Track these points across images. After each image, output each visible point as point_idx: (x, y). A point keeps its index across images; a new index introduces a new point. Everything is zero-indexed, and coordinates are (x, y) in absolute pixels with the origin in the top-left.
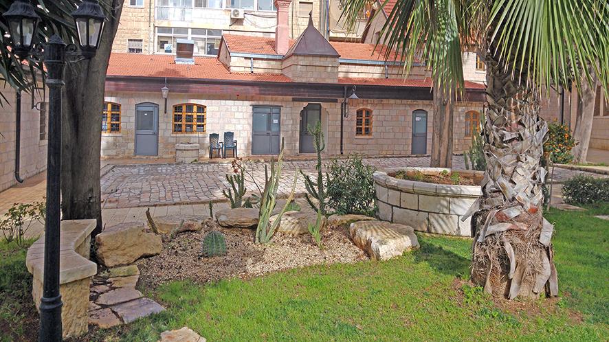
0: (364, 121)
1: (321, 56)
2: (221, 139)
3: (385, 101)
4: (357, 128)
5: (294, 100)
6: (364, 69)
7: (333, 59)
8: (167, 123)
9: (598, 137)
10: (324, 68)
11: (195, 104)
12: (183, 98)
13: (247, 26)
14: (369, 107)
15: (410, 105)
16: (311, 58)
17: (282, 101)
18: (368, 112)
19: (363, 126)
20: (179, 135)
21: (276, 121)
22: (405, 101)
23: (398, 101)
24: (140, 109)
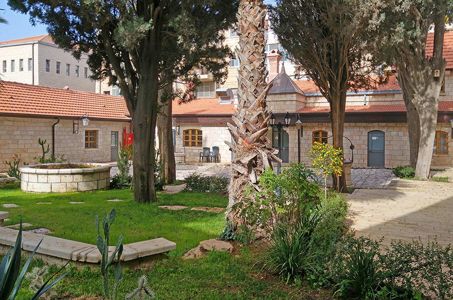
1: (280, 94)
7: (291, 95)
12: (195, 125)
15: (364, 127)
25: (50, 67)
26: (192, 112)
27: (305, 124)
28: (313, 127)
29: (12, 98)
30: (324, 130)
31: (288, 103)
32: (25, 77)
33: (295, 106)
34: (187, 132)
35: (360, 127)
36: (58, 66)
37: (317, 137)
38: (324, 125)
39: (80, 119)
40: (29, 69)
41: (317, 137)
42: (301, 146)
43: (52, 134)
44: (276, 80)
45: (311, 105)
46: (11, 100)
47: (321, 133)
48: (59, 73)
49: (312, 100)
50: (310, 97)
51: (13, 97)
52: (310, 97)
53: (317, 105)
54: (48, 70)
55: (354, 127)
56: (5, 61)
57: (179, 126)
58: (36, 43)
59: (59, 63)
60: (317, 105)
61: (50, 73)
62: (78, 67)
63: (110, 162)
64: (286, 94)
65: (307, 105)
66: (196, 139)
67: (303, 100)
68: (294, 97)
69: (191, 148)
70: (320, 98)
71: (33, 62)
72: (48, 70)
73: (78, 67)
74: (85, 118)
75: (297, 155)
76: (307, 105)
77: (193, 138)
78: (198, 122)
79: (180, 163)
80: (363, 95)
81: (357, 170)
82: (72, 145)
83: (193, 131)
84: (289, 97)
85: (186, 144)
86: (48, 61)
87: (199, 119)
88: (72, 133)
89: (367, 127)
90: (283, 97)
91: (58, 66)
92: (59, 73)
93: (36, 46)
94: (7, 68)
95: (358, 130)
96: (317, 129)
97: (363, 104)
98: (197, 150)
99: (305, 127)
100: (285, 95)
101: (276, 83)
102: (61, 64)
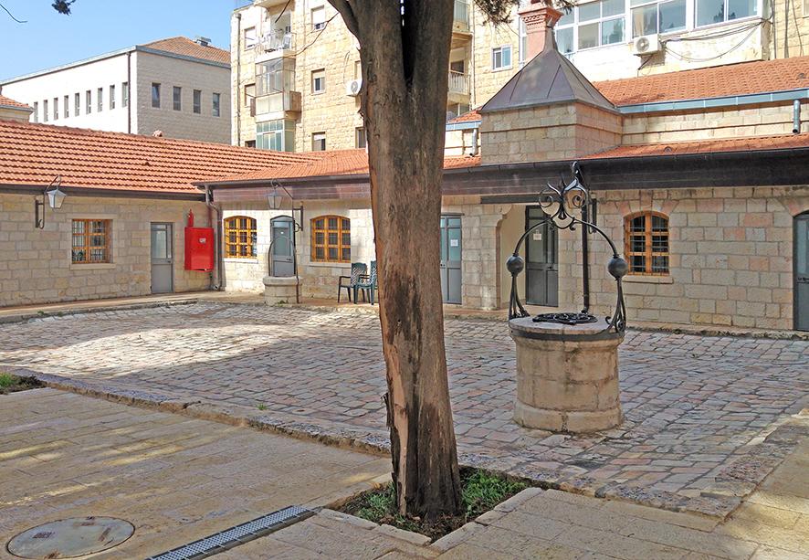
0: (648, 241)
1: (534, 108)
2: (517, 267)
3: (702, 192)
4: (666, 250)
5: (484, 201)
6: (729, 117)
7: (563, 109)
8: (304, 245)
9: (704, 533)
10: (541, 132)
11: (324, 217)
12: (330, 206)
13: (672, 64)
14: (656, 209)
15: (780, 199)
16: (515, 115)
17: (463, 205)
18: (661, 222)
19: (647, 254)
20: (320, 264)
21: (454, 243)
22: (765, 190)
23: (744, 191)
24: (277, 225)
25: (161, 97)
26: (323, 173)
27: (598, 194)
28: (626, 202)
29: (147, 164)
30: (638, 210)
31: (554, 133)
32: (114, 120)
33: (573, 143)
34: (317, 222)
35: (766, 200)
36: (177, 96)
37: (639, 234)
38: (656, 195)
39: (43, 190)
40: (124, 105)
41: (639, 234)
42: (591, 261)
43: (589, 242)
44: (528, 71)
45: (637, 140)
46: (147, 167)
47: (648, 222)
48: (179, 110)
49: (639, 125)
50: (632, 116)
51: (150, 163)
52: (632, 116)
53: (653, 139)
54: (156, 104)
55: (746, 199)
56: (89, 92)
57: (302, 209)
58: (133, 51)
59: (180, 88)
60: (653, 139)
61: (161, 109)
62: (219, 95)
63: (147, 296)
64: (548, 106)
65: (627, 140)
66: (326, 235)
67: (612, 124)
68: (572, 114)
69: (327, 264)
70: (661, 118)
71: (129, 88)
72: (156, 104)
73: (219, 95)
74: (54, 188)
75: (581, 287)
76: (627, 140)
77: (333, 239)
78: (337, 197)
79: (282, 302)
80: (790, 103)
81: (742, 342)
82: (34, 255)
83: (332, 220)
84: (556, 116)
85: (318, 255)
86: (156, 86)
87: (338, 187)
88: (31, 226)
89: (791, 199)
90: (542, 118)
91: (177, 96)
92: (179, 110)
93: (134, 56)
94: (92, 106)
95: (760, 207)
96: (636, 209)
97: (789, 130)
98: (339, 268)
99: (603, 202)
100: (545, 111)
101: (528, 81)
102: (182, 90)
